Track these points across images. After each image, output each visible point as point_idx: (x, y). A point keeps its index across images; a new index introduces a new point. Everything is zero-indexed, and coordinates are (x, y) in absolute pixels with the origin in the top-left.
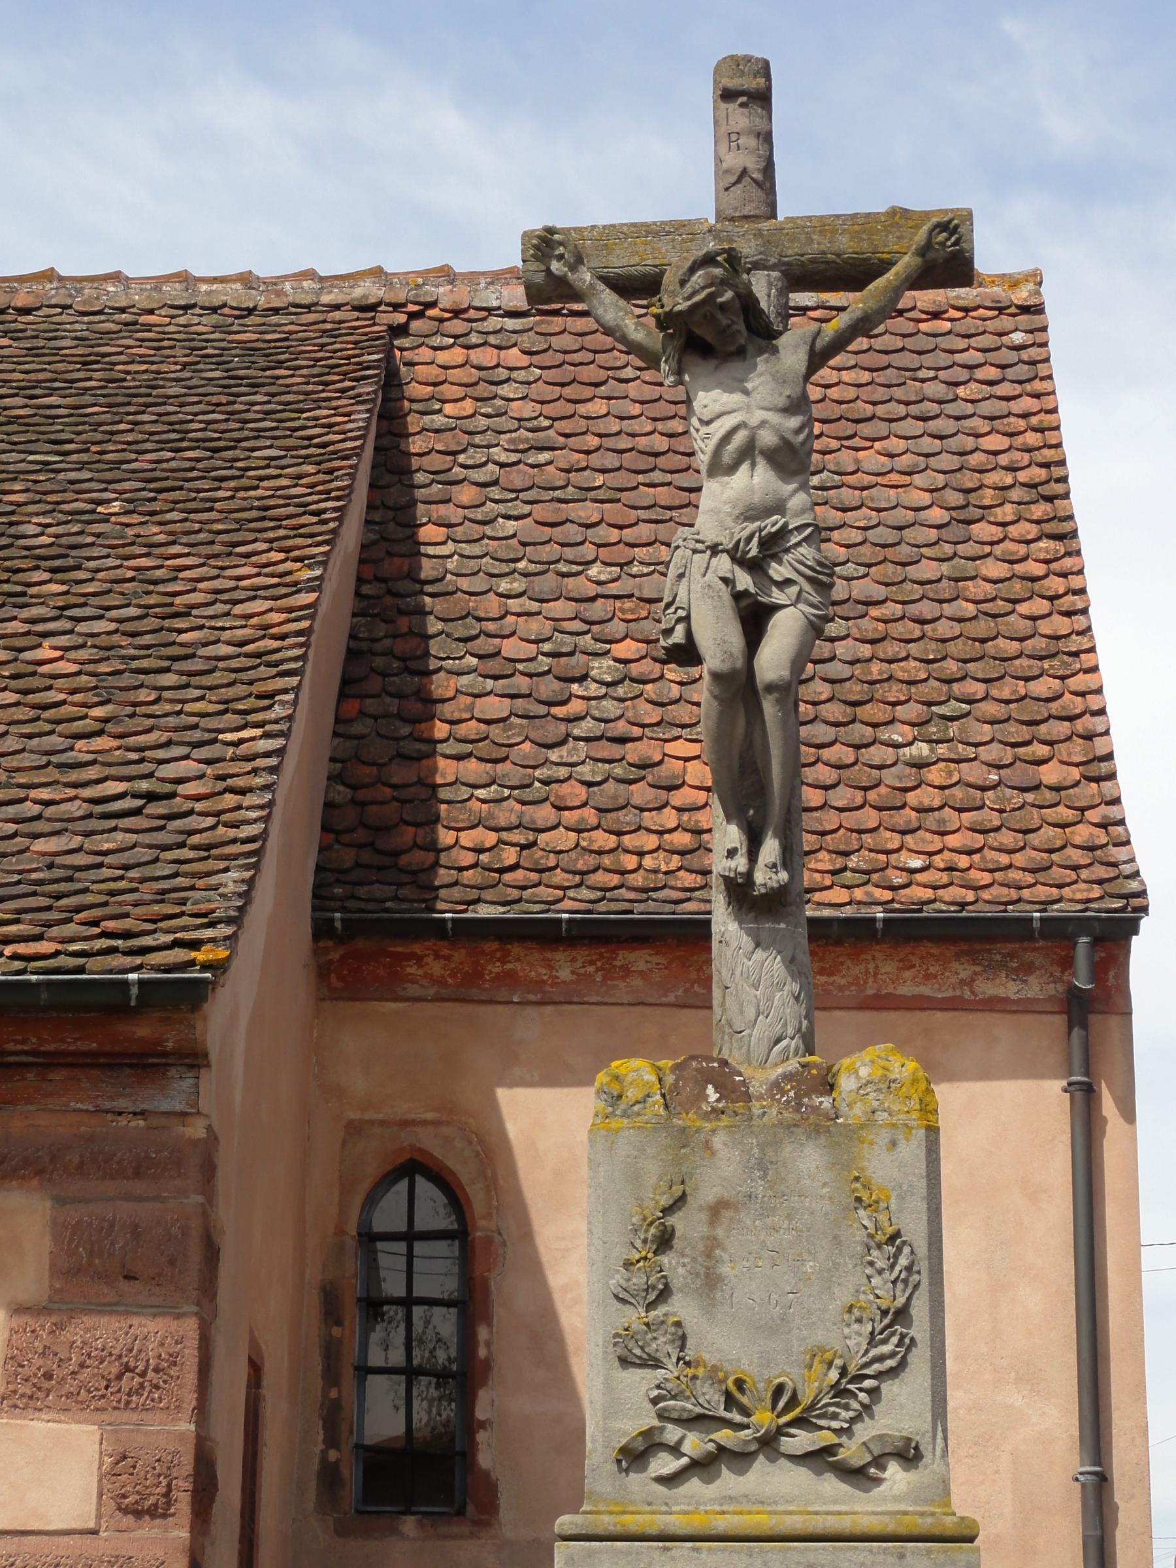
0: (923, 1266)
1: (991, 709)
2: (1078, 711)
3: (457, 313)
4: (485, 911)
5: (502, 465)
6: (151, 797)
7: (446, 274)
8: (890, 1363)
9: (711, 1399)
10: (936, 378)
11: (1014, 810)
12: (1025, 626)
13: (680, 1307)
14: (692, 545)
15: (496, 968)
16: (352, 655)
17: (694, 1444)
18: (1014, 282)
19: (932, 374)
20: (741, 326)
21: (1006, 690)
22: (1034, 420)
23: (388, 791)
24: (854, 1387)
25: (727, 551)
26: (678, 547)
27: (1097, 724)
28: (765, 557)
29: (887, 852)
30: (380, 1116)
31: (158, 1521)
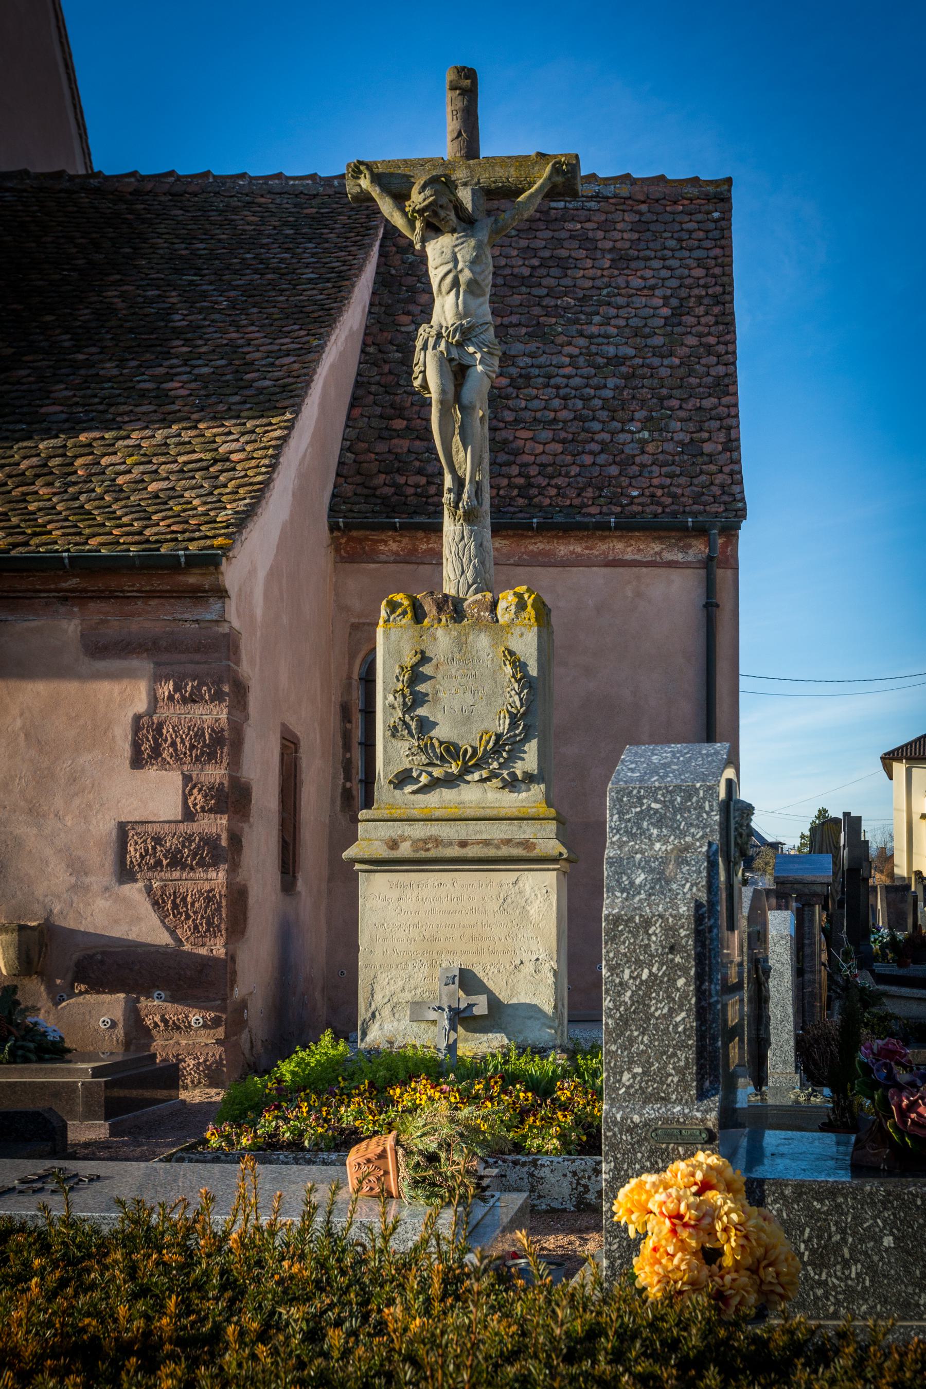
1: (682, 414)
15: (424, 546)
16: (358, 384)
23: (373, 456)
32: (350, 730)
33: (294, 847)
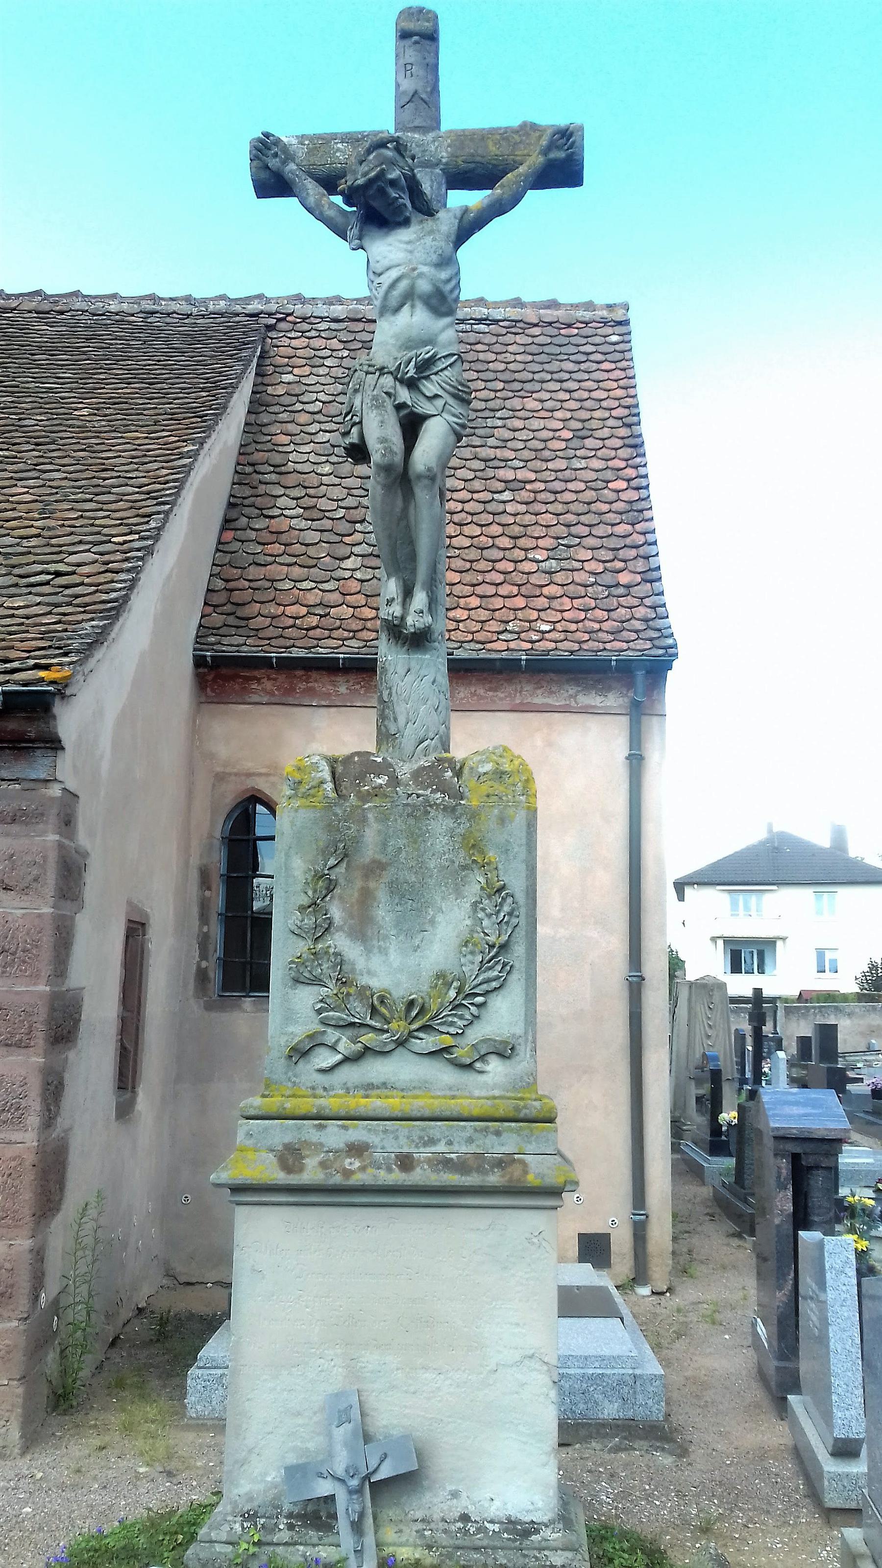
0: (523, 911)
1: (591, 542)
2: (641, 543)
3: (304, 319)
4: (296, 653)
5: (324, 403)
6: (58, 574)
7: (299, 298)
8: (494, 984)
9: (359, 1010)
10: (568, 359)
11: (603, 598)
12: (612, 496)
13: (339, 942)
14: (365, 368)
17: (346, 1046)
18: (610, 307)
19: (566, 357)
20: (409, 205)
21: (600, 531)
22: (621, 383)
23: (247, 584)
24: (470, 998)
25: (391, 373)
26: (356, 370)
27: (652, 550)
28: (419, 379)
29: (530, 622)
30: (235, 770)
31: (23, 1051)
32: (209, 899)
33: (136, 1054)
